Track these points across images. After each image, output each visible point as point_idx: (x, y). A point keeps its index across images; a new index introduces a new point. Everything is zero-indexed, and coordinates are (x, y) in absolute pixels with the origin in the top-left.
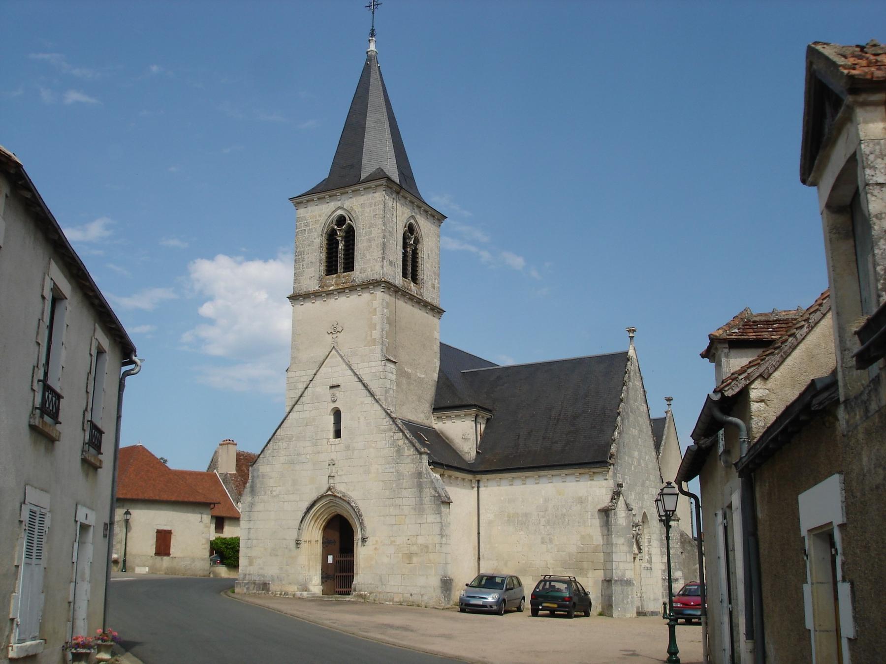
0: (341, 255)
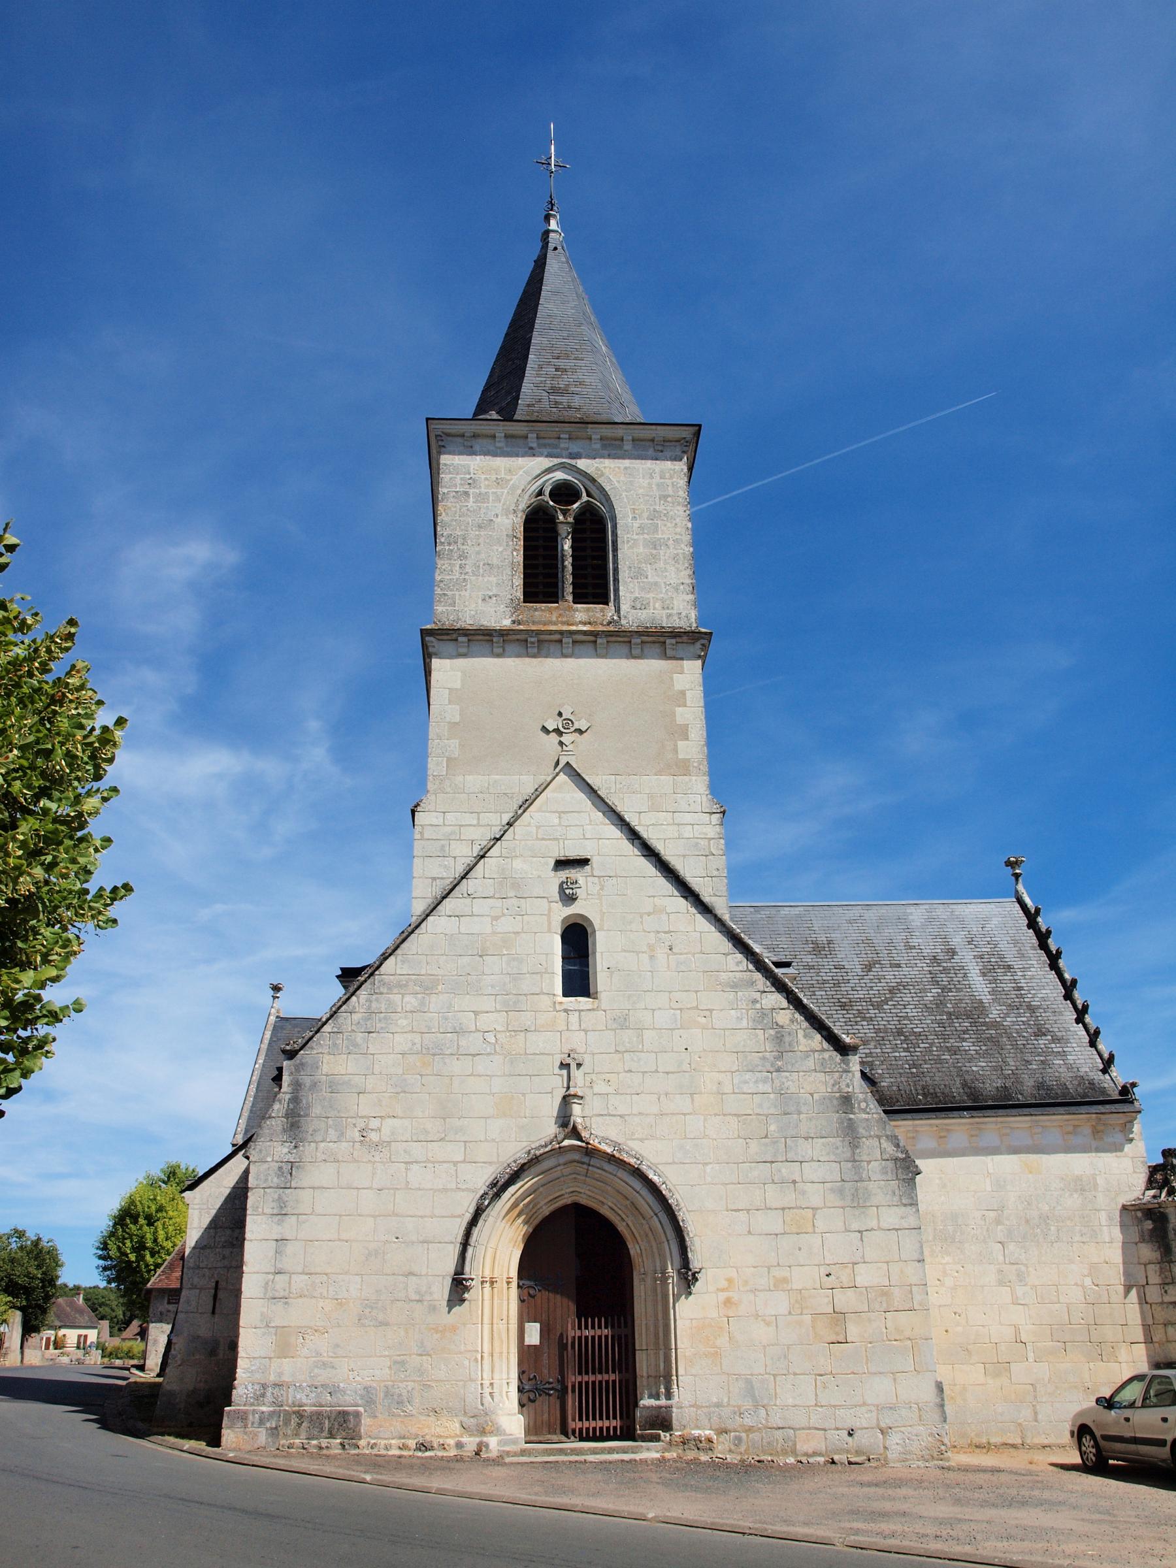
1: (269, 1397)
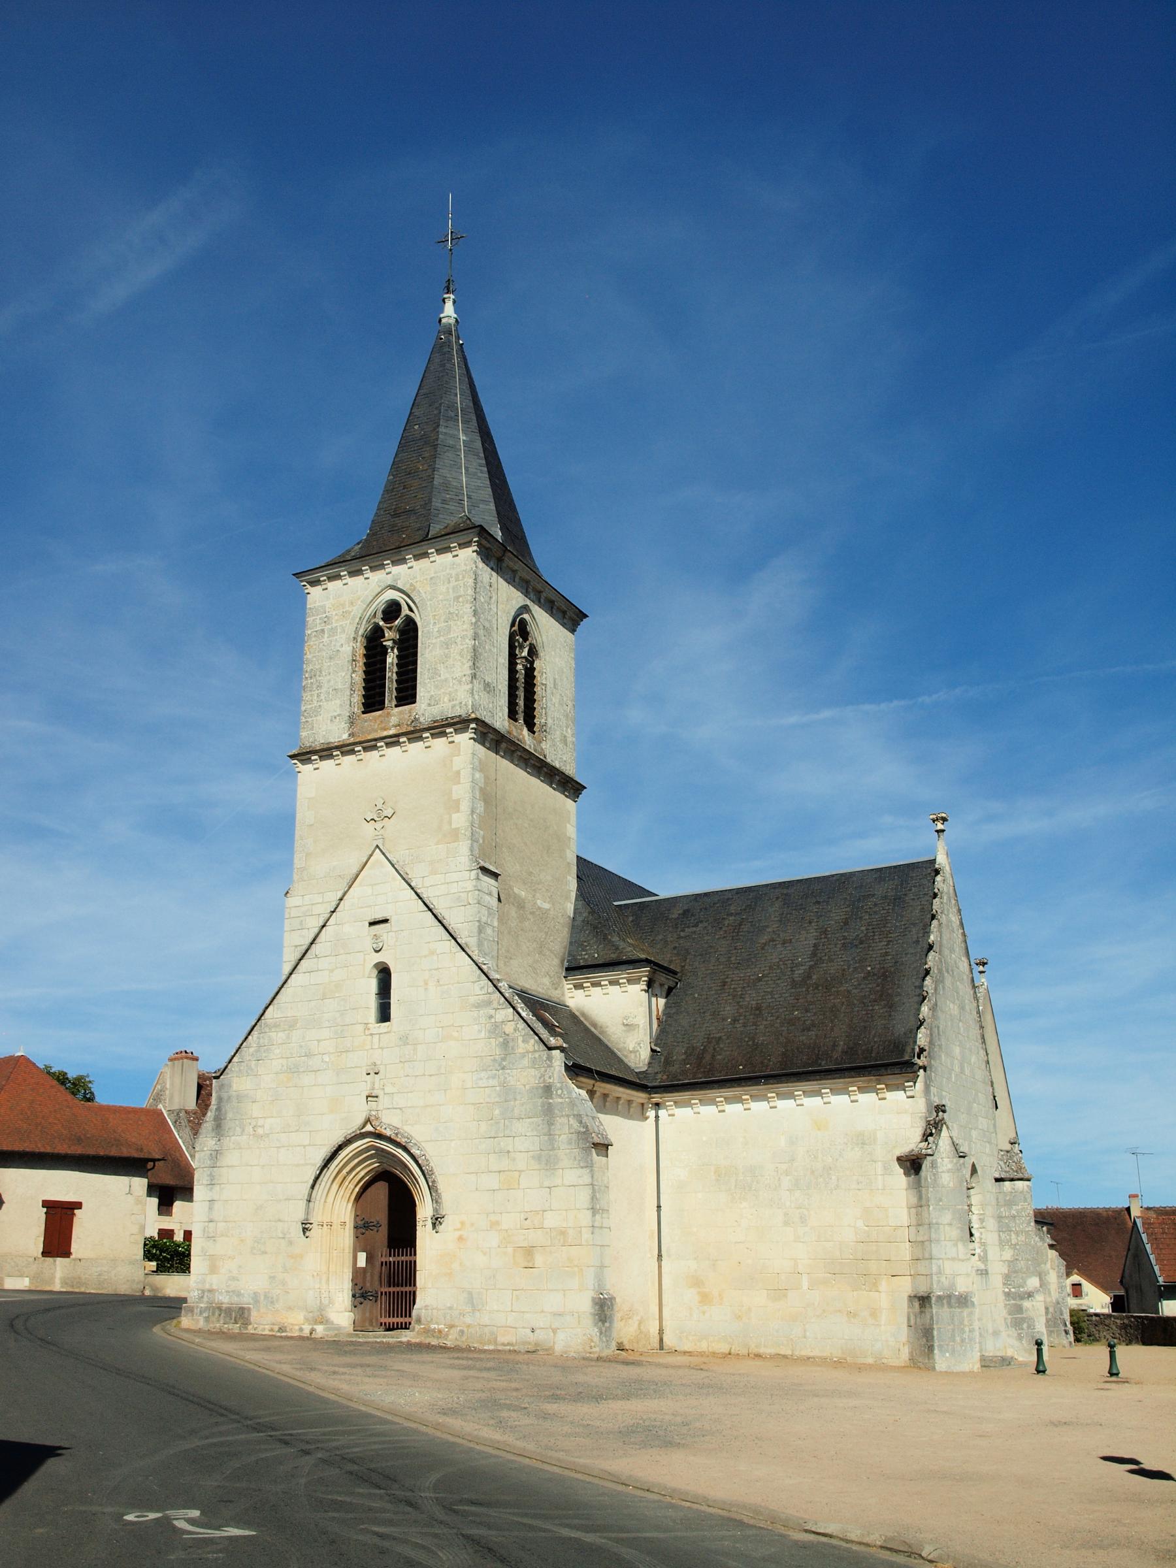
0: (391, 674)
1: (205, 1299)
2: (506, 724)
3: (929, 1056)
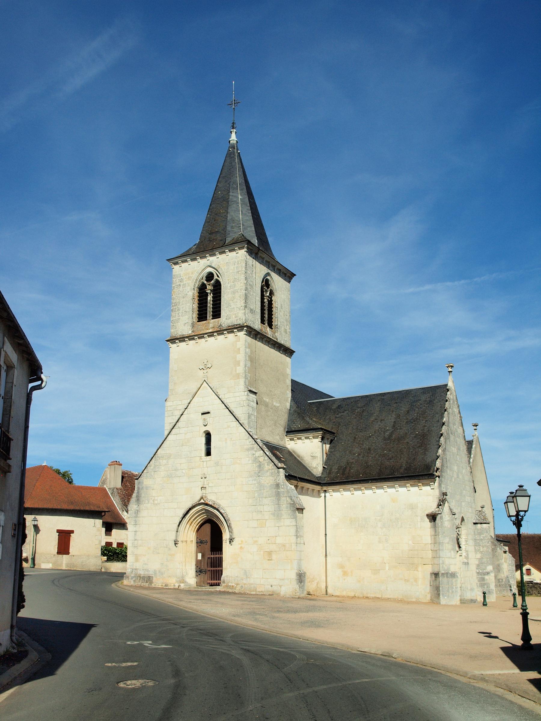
0: (210, 305)
1: (134, 573)
2: (260, 326)
3: (441, 471)
